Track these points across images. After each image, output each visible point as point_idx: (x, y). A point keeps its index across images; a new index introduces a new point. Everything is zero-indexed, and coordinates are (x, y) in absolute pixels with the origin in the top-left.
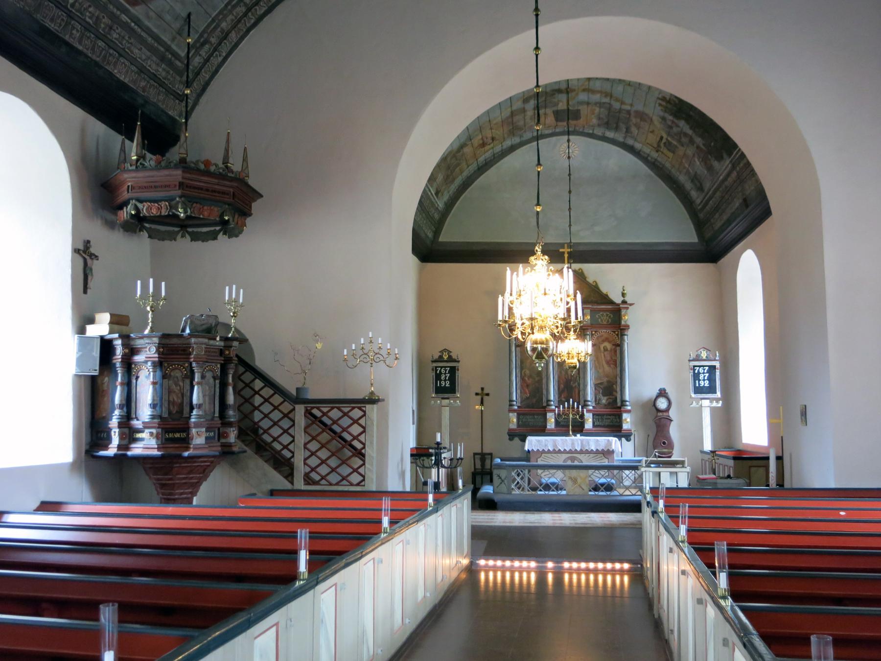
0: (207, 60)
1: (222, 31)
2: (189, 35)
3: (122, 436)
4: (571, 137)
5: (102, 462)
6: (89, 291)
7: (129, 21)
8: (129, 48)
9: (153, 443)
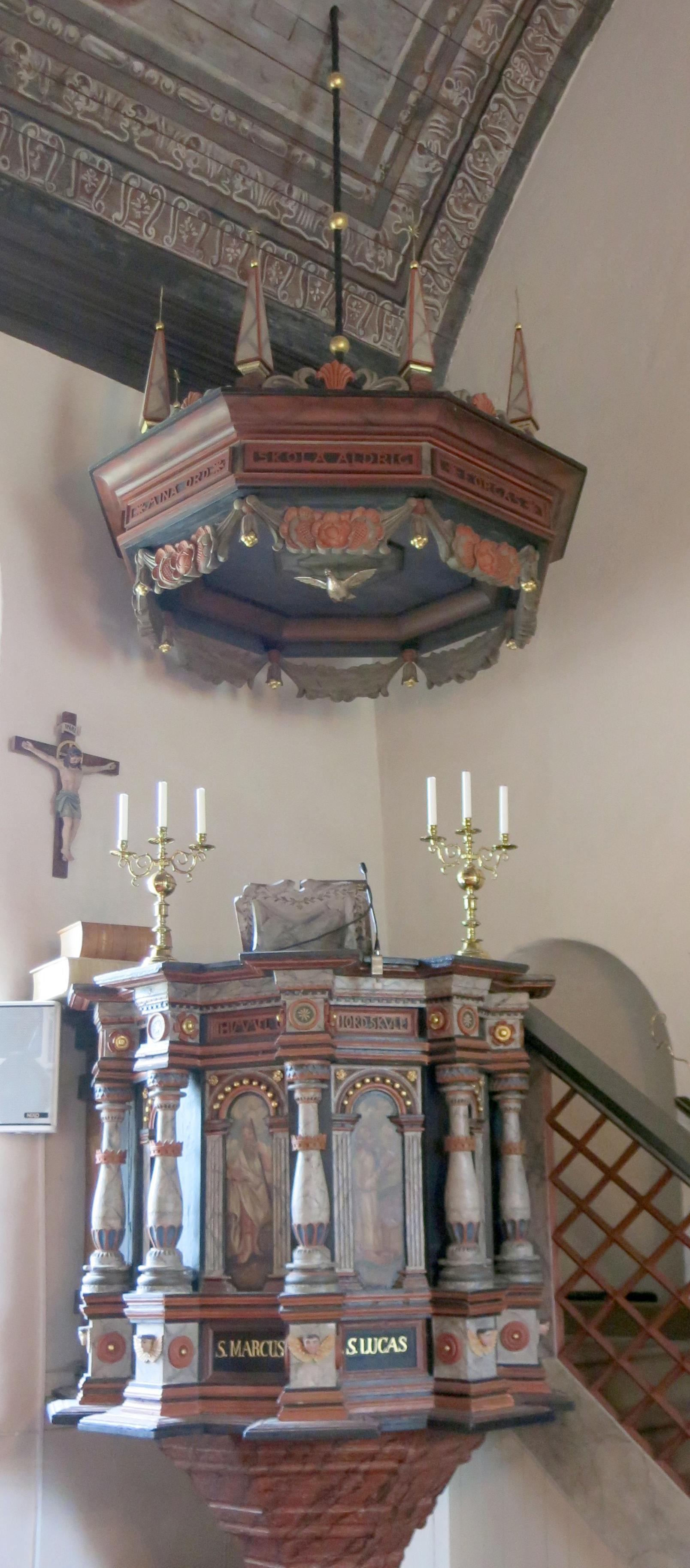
0: (455, 165)
1: (476, 60)
2: (335, 68)
7: (121, 55)
8: (147, 142)
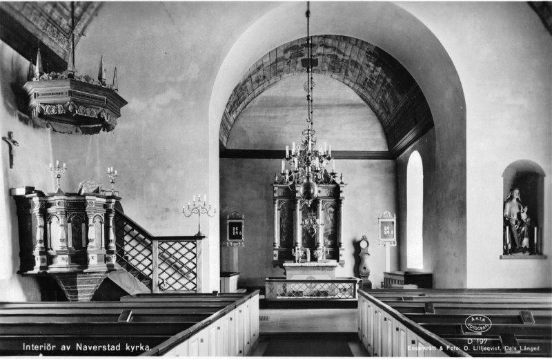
3: (43, 261)
4: (315, 76)
5: (382, 286)
6: (13, 166)
9: (65, 263)
